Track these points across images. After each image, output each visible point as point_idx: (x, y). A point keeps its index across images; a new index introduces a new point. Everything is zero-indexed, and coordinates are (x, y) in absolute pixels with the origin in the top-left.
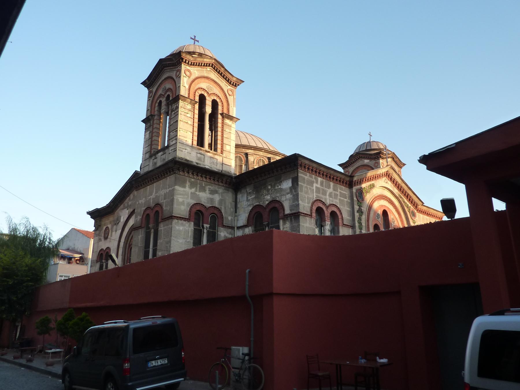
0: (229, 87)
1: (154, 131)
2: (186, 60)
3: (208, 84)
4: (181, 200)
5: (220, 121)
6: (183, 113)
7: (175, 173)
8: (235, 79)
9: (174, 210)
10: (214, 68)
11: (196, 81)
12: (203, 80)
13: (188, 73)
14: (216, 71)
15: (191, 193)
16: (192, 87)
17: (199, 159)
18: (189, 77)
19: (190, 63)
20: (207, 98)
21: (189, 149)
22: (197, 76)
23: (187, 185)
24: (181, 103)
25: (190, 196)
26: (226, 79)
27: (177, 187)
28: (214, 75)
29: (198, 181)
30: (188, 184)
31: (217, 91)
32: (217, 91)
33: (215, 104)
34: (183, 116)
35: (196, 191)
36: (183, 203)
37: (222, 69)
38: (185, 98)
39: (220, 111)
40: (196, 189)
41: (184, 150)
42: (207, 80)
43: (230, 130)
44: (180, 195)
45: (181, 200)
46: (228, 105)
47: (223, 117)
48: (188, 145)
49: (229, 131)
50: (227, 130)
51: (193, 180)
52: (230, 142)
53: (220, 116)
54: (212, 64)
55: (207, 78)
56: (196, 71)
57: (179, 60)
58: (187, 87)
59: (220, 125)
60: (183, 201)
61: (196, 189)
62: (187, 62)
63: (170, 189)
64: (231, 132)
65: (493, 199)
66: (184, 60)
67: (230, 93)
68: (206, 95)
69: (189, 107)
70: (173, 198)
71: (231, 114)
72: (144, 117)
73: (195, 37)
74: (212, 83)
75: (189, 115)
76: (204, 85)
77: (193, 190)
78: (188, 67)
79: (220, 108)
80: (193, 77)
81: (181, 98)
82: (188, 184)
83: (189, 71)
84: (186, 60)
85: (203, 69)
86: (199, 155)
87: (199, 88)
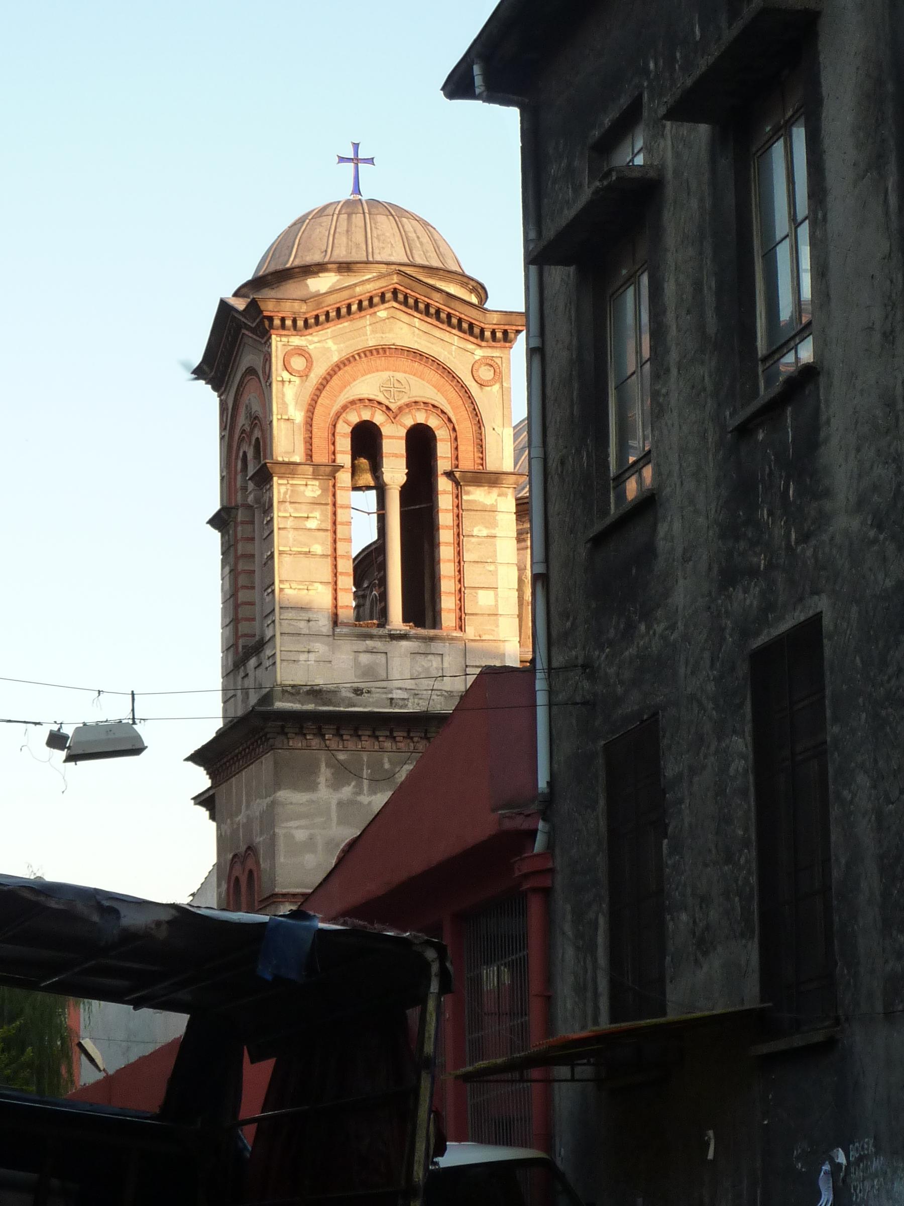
0: (479, 353)
1: (240, 568)
2: (283, 320)
3: (385, 375)
4: (301, 835)
5: (445, 501)
6: (290, 523)
7: (272, 748)
8: (495, 318)
9: (279, 871)
10: (405, 303)
11: (335, 381)
12: (364, 362)
13: (298, 363)
14: (416, 308)
15: (340, 804)
16: (319, 410)
17: (369, 672)
18: (304, 375)
19: (300, 323)
20: (385, 431)
21: (320, 648)
22: (335, 358)
23: (322, 780)
24: (280, 488)
25: (334, 815)
26: (460, 327)
27: (283, 795)
28: (406, 330)
29: (365, 757)
30: (324, 774)
31: (423, 387)
32: (423, 387)
33: (420, 443)
34: (291, 535)
35: (359, 792)
36: (309, 845)
37: (437, 296)
38: (290, 468)
39: (443, 464)
40: (359, 786)
41: (303, 657)
42: (381, 362)
43: (493, 524)
44: (299, 817)
45: (301, 835)
46: (479, 424)
47: (457, 483)
48: (317, 635)
49: (485, 532)
50: (476, 529)
51: (342, 756)
52: (494, 573)
53: (444, 485)
54: (395, 292)
55: (381, 351)
56: (327, 345)
57: (262, 322)
58: (299, 416)
59: (445, 519)
60: (311, 838)
61: (359, 786)
62: (289, 323)
63: (269, 800)
64: (496, 532)
65: (172, 1025)
66: (277, 322)
67: (486, 374)
68: (379, 418)
69: (313, 490)
70: (274, 834)
71: (491, 466)
72: (215, 506)
73: (356, 146)
74: (404, 362)
75: (312, 524)
76: (368, 385)
77: (347, 792)
78: (296, 341)
79: (443, 450)
80: (319, 371)
81: (277, 469)
82: (324, 774)
83: (301, 352)
84: (283, 320)
85: (360, 323)
86: (365, 659)
87: (353, 402)
